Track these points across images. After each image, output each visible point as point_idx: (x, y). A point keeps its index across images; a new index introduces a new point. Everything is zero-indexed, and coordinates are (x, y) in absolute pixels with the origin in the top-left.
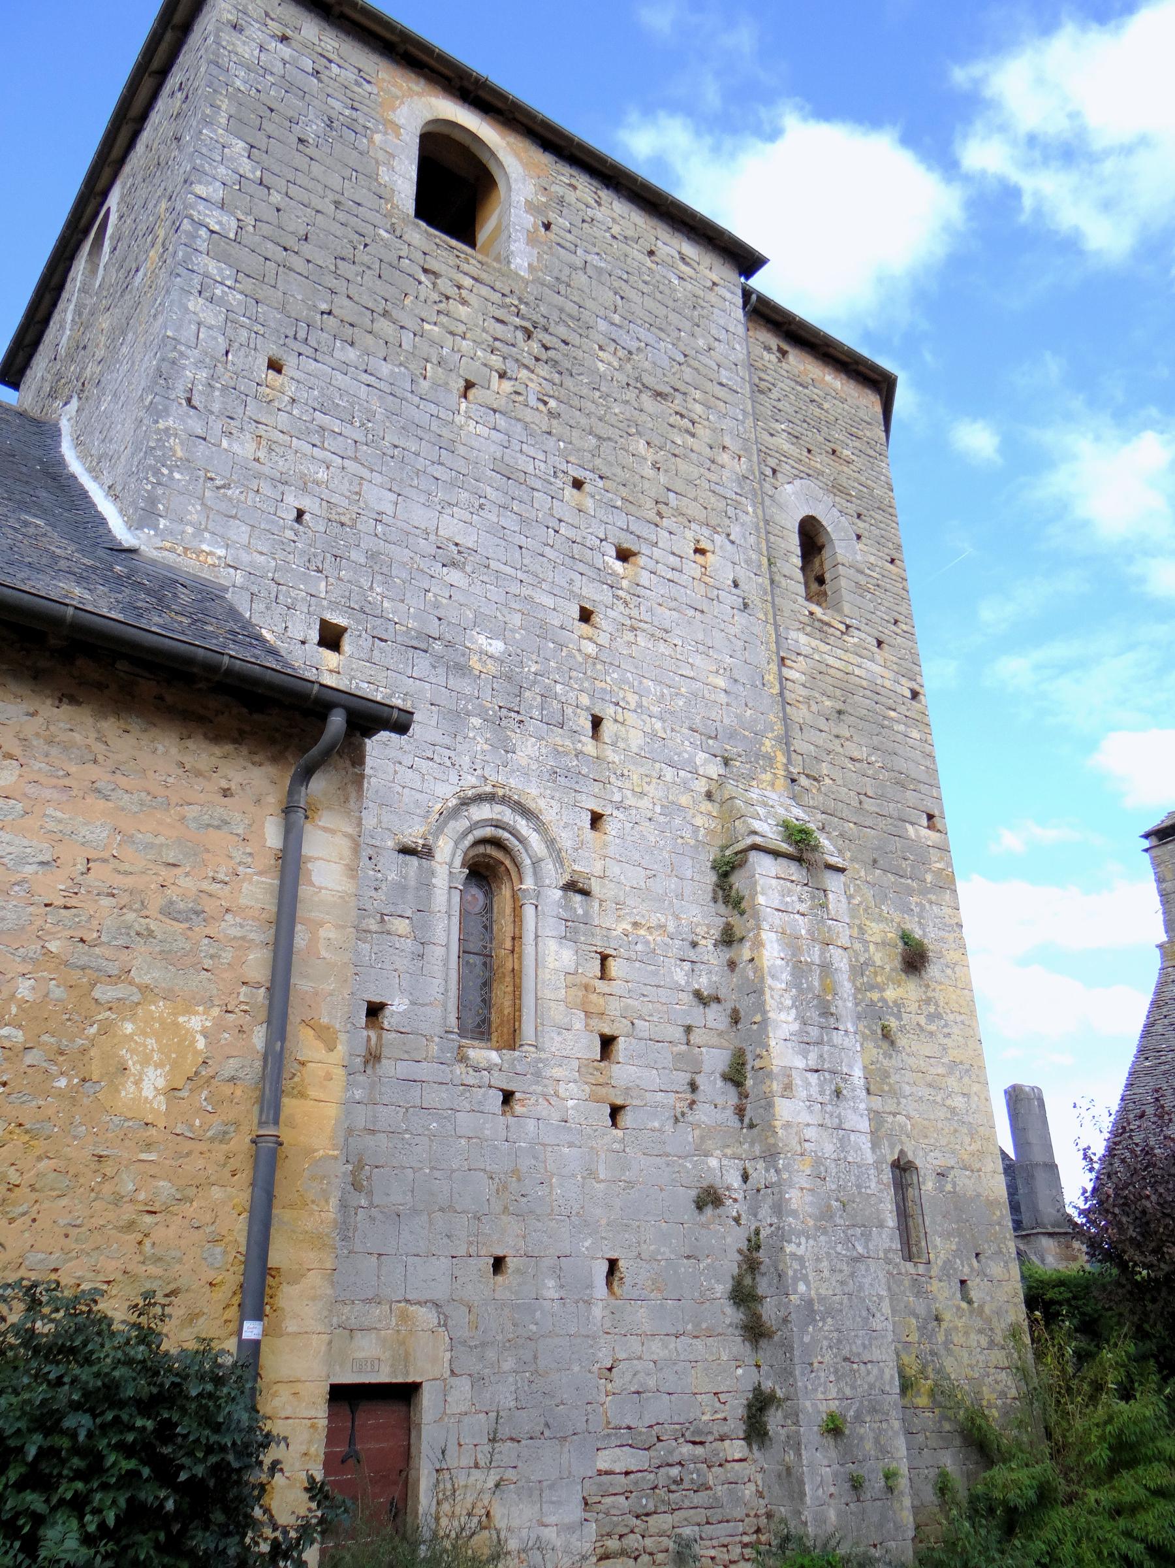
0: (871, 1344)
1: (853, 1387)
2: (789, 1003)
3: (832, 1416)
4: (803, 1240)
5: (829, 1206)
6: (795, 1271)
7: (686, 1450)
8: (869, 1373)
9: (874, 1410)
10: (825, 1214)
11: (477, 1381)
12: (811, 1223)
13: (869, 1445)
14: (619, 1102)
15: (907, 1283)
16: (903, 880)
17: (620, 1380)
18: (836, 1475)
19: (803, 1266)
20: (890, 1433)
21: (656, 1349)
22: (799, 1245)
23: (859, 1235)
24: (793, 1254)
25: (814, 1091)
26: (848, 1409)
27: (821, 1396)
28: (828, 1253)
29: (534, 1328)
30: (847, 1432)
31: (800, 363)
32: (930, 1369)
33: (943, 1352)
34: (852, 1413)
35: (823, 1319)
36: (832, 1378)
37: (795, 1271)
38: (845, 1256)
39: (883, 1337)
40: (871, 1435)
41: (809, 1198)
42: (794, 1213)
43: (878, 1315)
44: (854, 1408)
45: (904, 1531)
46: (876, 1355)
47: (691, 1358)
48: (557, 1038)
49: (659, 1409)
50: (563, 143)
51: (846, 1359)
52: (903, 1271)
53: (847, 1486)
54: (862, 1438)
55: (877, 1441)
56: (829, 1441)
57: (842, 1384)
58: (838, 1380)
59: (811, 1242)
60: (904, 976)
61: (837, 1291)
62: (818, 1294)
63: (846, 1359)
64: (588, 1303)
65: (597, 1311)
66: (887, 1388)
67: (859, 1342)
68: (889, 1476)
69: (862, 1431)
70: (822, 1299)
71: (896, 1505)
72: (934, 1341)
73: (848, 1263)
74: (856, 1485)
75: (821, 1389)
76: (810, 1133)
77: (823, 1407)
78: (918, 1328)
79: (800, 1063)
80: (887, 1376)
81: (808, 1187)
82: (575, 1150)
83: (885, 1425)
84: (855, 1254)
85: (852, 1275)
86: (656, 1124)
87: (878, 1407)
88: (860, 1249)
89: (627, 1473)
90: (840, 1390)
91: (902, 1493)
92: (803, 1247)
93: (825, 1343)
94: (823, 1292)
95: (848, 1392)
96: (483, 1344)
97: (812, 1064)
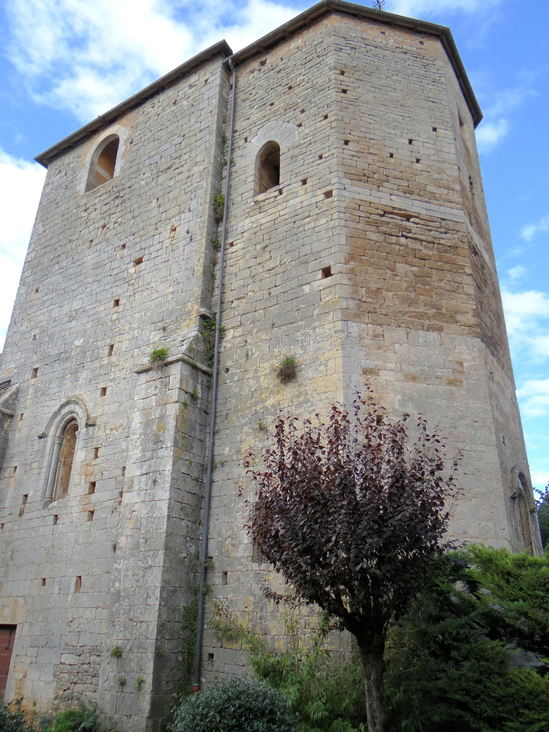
0: (145, 612)
1: (131, 634)
2: (139, 444)
3: (117, 648)
4: (122, 561)
5: (138, 542)
6: (115, 577)
7: (93, 658)
8: (141, 627)
9: (140, 647)
10: (136, 546)
11: (31, 624)
12: (128, 551)
13: (133, 665)
14: (92, 510)
15: (251, 576)
16: (295, 325)
17: (74, 626)
18: (114, 676)
19: (119, 574)
20: (146, 660)
21: (89, 614)
22: (120, 564)
23: (151, 555)
24: (116, 569)
25: (143, 485)
26: (127, 644)
27: (115, 638)
28: (133, 567)
29: (49, 605)
30: (124, 656)
31: (272, 58)
32: (258, 628)
33: (269, 617)
34: (128, 647)
35: (124, 600)
36: (122, 629)
37: (115, 577)
38: (142, 567)
39: (152, 608)
40: (136, 659)
41: (129, 539)
42: (121, 548)
43: (152, 597)
44: (130, 645)
45: (143, 713)
46: (147, 618)
47: (101, 618)
48: (74, 490)
49: (85, 640)
50: (157, 88)
51: (131, 620)
52: (250, 569)
53: (118, 683)
54: (131, 661)
55: (138, 663)
56: (115, 660)
57: (126, 632)
58: (124, 630)
59: (126, 562)
60: (283, 386)
61: (134, 585)
62: (124, 587)
63: (131, 620)
64: (67, 595)
65: (70, 598)
66: (149, 636)
67: (139, 611)
68: (141, 682)
69: (132, 656)
70: (125, 589)
71: (141, 698)
72: (264, 610)
73: (142, 571)
74: (123, 683)
75: (115, 634)
76: (136, 507)
77: (115, 643)
78: (254, 603)
79: (138, 473)
80: (150, 629)
81: (130, 534)
82: (73, 534)
83: (144, 655)
84: (147, 565)
85: (144, 577)
86: (104, 516)
87: (142, 645)
88: (150, 563)
89: (70, 665)
90: (124, 635)
91: (145, 692)
92: (121, 565)
93: (122, 612)
94: (126, 586)
95: (128, 636)
96: (34, 611)
97: (144, 471)
